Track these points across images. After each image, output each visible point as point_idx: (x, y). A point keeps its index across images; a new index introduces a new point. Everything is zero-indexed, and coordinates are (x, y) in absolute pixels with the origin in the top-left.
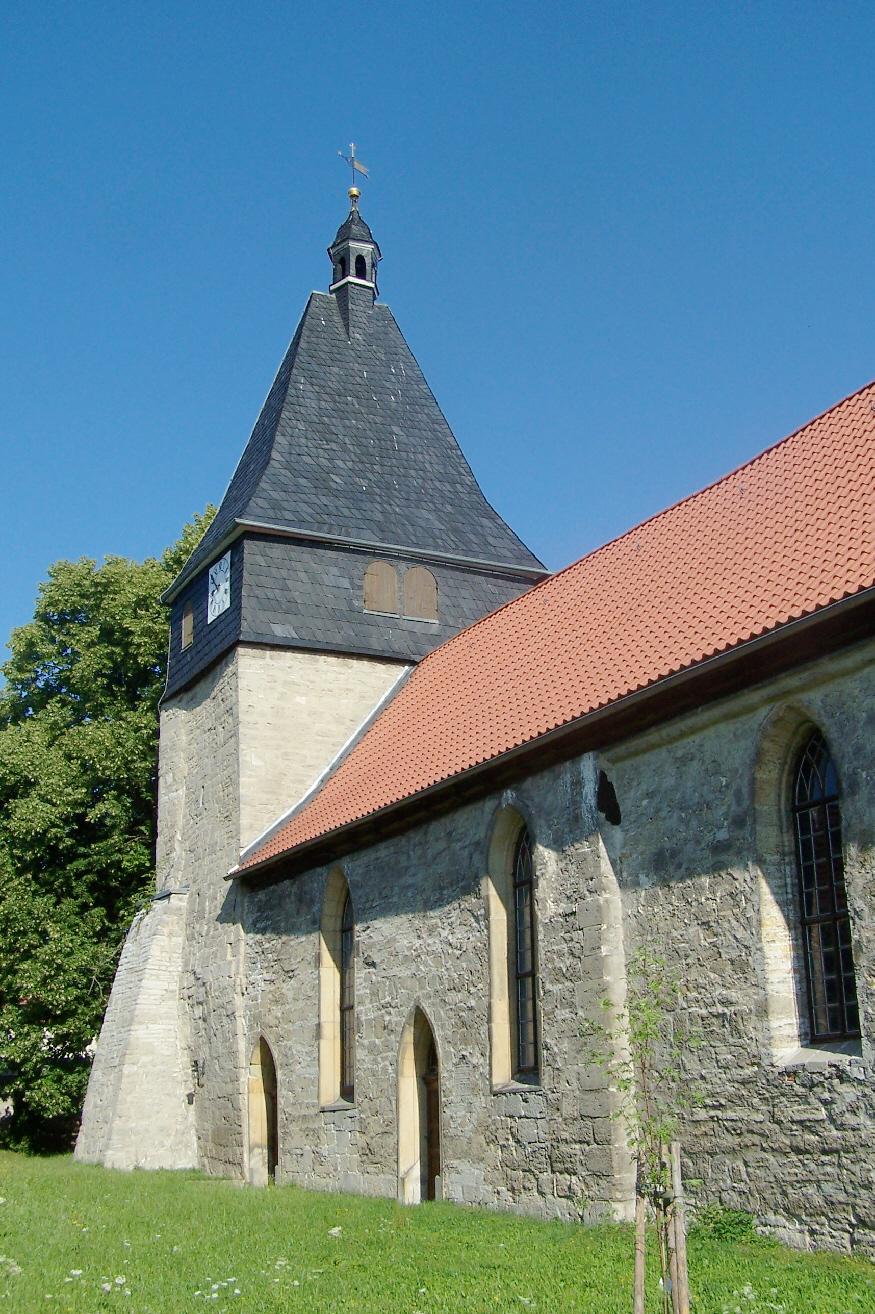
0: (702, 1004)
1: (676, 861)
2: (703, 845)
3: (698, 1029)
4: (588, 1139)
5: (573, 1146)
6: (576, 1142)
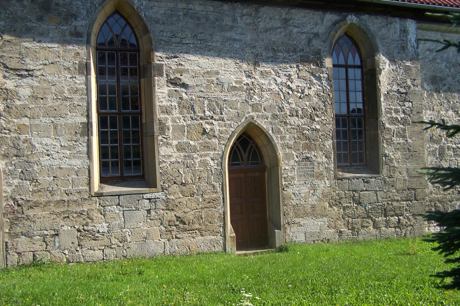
0: (453, 143)
1: (443, 82)
2: (456, 80)
3: (451, 153)
4: (411, 199)
5: (402, 203)
6: (403, 201)
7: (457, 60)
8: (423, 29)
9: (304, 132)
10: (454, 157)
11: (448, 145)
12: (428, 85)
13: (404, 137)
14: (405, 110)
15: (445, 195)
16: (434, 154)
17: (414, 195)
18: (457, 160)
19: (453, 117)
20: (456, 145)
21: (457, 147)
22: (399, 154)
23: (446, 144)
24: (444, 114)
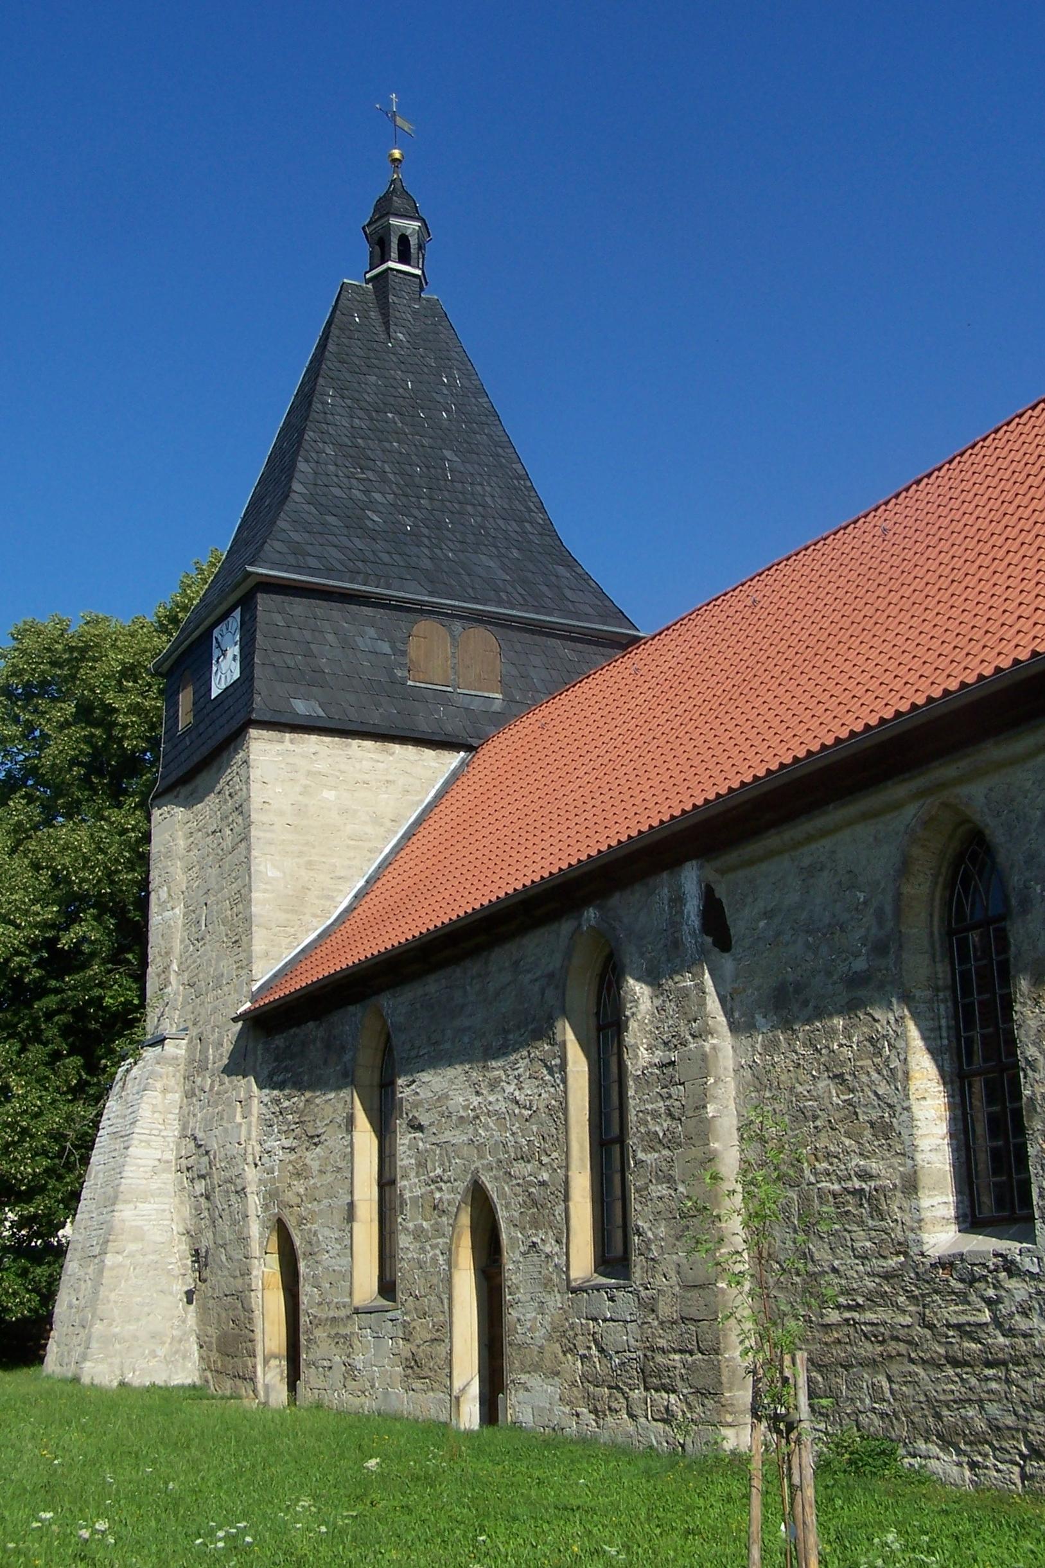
0: (834, 1178)
6: (675, 1351)
7: (835, 916)
8: (733, 869)
9: (530, 1190)
10: (839, 1222)
11: (819, 1186)
12: (765, 1017)
13: (670, 1180)
14: (672, 1109)
15: (826, 1344)
16: (788, 1218)
17: (695, 1338)
18: (849, 1232)
19: (830, 1097)
20: (840, 1183)
21: (845, 1189)
22: (662, 1231)
23: (813, 1184)
24: (805, 1093)
